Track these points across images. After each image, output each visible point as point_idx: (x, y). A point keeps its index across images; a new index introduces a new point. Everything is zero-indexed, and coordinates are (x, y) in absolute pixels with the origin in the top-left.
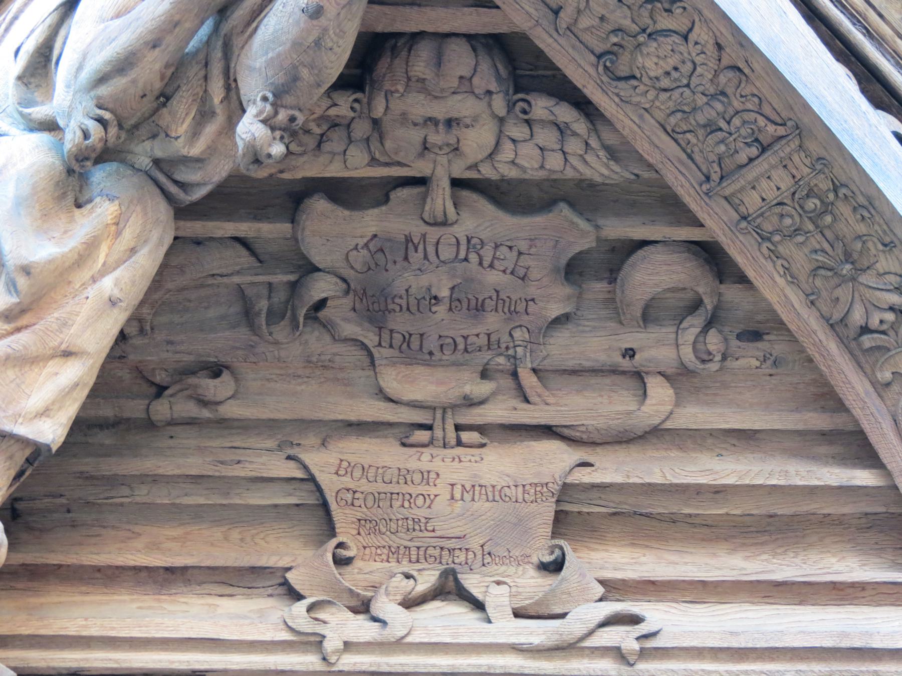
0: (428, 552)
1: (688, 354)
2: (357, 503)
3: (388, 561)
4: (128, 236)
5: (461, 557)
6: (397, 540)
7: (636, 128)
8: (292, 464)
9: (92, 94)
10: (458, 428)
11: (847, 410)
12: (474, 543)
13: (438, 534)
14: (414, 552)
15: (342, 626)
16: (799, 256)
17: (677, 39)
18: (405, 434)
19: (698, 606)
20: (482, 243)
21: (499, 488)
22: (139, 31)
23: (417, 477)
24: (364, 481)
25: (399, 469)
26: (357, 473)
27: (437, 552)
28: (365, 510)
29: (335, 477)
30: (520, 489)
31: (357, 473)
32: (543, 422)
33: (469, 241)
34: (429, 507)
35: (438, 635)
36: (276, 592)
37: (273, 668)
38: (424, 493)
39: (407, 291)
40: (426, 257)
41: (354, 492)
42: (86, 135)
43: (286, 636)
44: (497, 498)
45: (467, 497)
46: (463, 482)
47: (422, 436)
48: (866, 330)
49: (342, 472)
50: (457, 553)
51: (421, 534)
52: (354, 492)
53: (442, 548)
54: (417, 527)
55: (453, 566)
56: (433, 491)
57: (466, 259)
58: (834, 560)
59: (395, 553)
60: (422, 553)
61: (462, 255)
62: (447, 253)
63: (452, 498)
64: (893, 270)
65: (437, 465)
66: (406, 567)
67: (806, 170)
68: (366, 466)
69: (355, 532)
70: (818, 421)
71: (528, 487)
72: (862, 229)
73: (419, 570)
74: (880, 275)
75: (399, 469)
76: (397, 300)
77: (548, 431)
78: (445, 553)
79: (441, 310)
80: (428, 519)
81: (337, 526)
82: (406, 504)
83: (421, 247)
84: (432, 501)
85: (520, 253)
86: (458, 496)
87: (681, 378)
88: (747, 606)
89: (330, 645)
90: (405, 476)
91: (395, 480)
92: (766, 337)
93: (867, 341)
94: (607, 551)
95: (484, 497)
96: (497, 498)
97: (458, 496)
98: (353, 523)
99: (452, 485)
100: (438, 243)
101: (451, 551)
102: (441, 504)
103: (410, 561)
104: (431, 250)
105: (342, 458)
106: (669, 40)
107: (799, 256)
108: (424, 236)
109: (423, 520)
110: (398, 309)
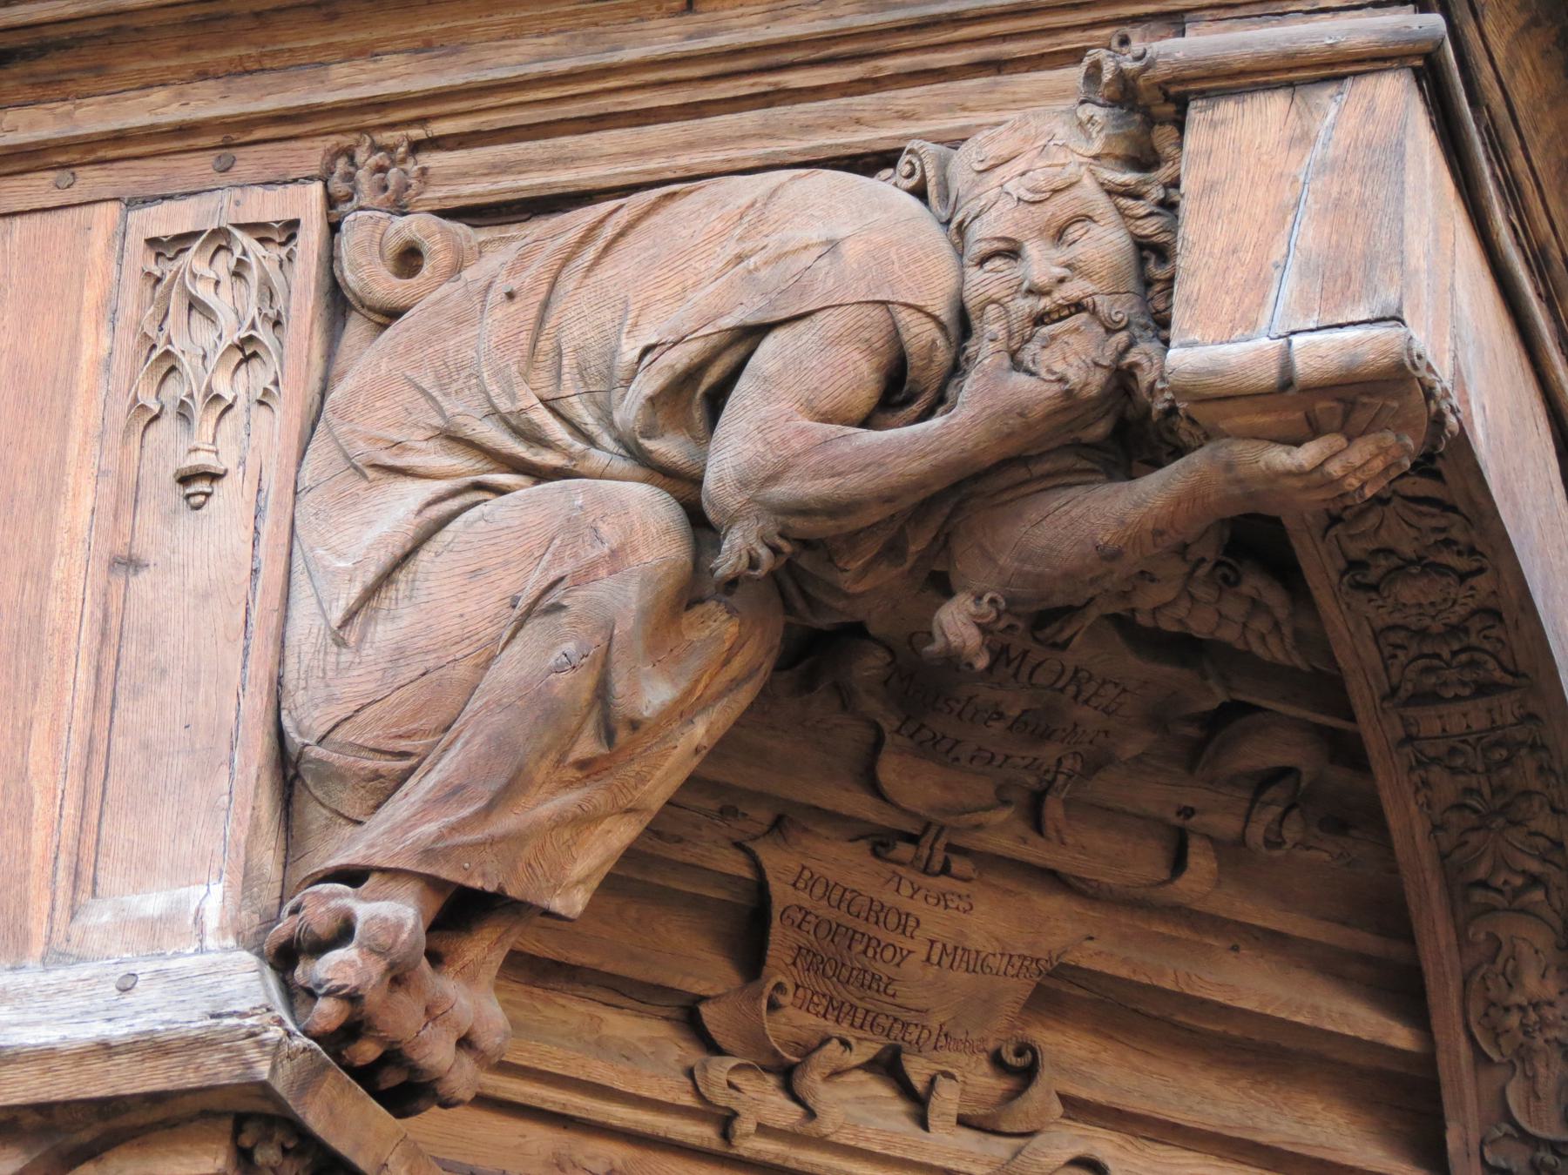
0: (879, 1020)
1: (1256, 833)
2: (805, 926)
3: (824, 1016)
4: (737, 664)
5: (913, 1033)
6: (845, 993)
7: (1347, 636)
8: (741, 857)
9: (780, 518)
10: (951, 848)
11: (1413, 942)
12: (934, 1025)
13: (898, 1001)
14: (860, 1014)
15: (764, 1101)
16: (1447, 788)
17: (1452, 580)
18: (881, 843)
19: (1158, 1146)
20: (1090, 678)
21: (983, 955)
22: (878, 481)
23: (893, 920)
24: (824, 902)
25: (872, 901)
26: (819, 890)
27: (887, 1023)
28: (812, 938)
29: (790, 889)
30: (1006, 959)
31: (819, 890)
32: (1051, 865)
33: (1076, 671)
34: (898, 965)
35: (868, 1139)
36: (674, 1015)
37: (662, 1134)
38: (898, 945)
39: (970, 698)
40: (1015, 676)
41: (807, 913)
42: (754, 563)
43: (687, 1100)
44: (978, 968)
45: (946, 961)
46: (945, 940)
47: (904, 850)
48: (1484, 884)
49: (801, 885)
50: (912, 1028)
51: (877, 996)
52: (807, 913)
53: (896, 1020)
54: (874, 986)
55: (900, 1043)
56: (908, 944)
57: (1062, 690)
58: (1319, 1107)
59: (835, 1008)
60: (869, 1019)
61: (1060, 684)
62: (1041, 678)
63: (928, 959)
64: (1547, 832)
65: (917, 907)
66: (844, 1030)
67: (1511, 719)
68: (832, 883)
69: (789, 960)
70: (1369, 943)
71: (1015, 960)
72: (1536, 785)
73: (859, 1039)
74: (1532, 834)
75: (872, 901)
76: (952, 703)
77: (1054, 879)
78: (898, 1026)
79: (998, 727)
80: (891, 980)
81: (771, 946)
82: (870, 953)
83: (1016, 663)
84: (903, 958)
85: (1124, 690)
86: (935, 959)
87: (1232, 852)
88: (1212, 1160)
89: (745, 1125)
90: (878, 912)
91: (863, 914)
92: (1354, 833)
93: (1478, 896)
94: (1063, 1033)
95: (964, 965)
96: (978, 968)
97: (935, 959)
98: (791, 948)
99: (932, 942)
100: (1039, 665)
101: (905, 1025)
102: (913, 964)
103: (852, 1025)
104: (1025, 670)
105: (807, 864)
106: (1444, 581)
107: (1447, 788)
108: (1025, 653)
109: (885, 979)
110: (947, 710)
